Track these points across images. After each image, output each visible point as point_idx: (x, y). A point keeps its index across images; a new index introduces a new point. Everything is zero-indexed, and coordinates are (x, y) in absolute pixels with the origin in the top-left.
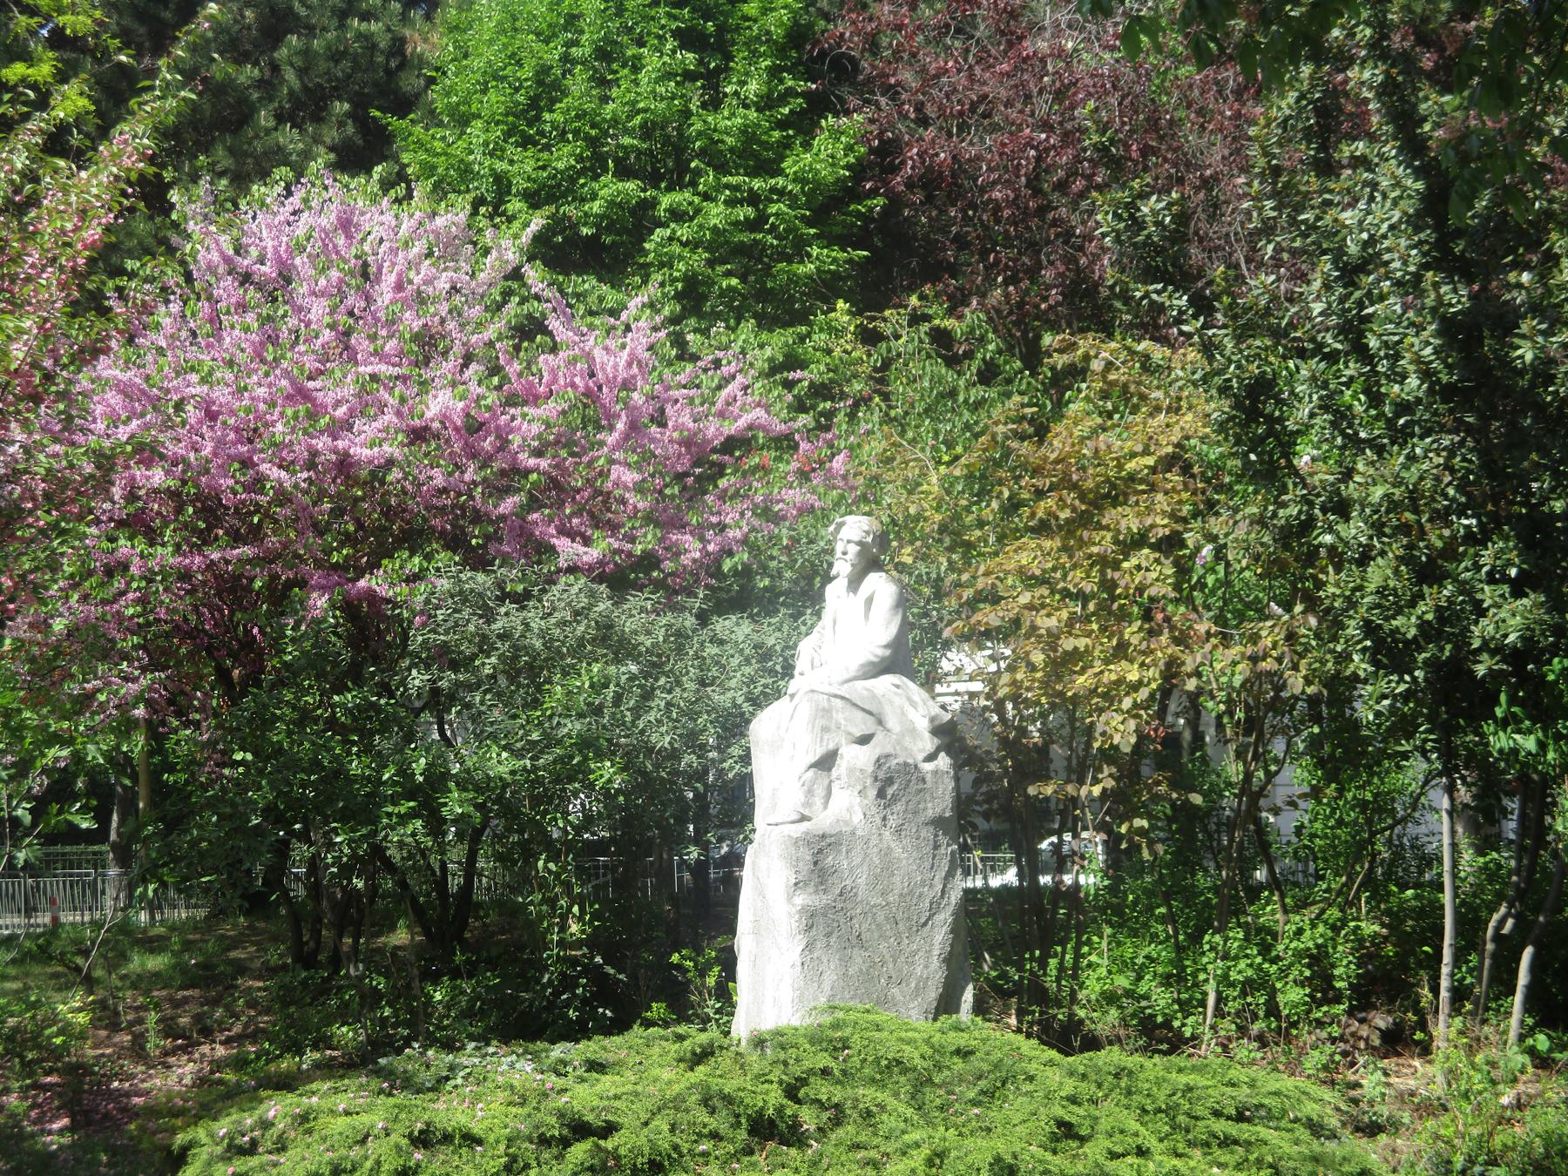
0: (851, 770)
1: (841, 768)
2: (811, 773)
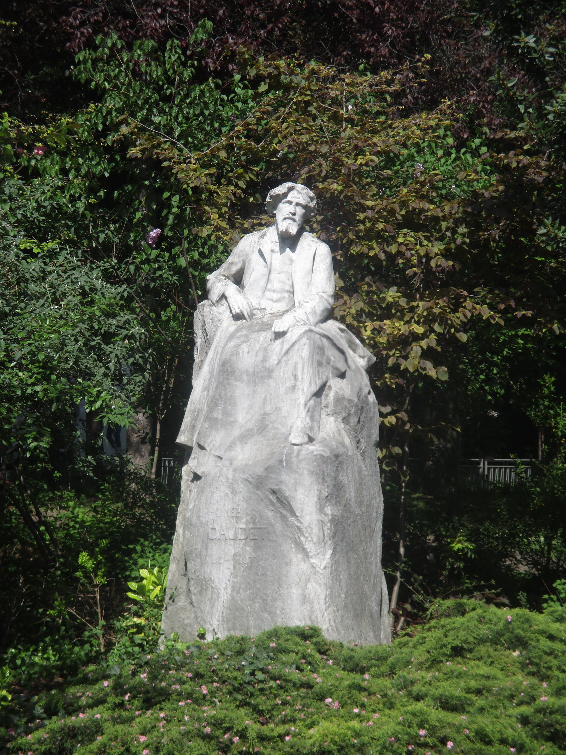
0: (339, 400)
1: (330, 396)
2: (312, 402)
